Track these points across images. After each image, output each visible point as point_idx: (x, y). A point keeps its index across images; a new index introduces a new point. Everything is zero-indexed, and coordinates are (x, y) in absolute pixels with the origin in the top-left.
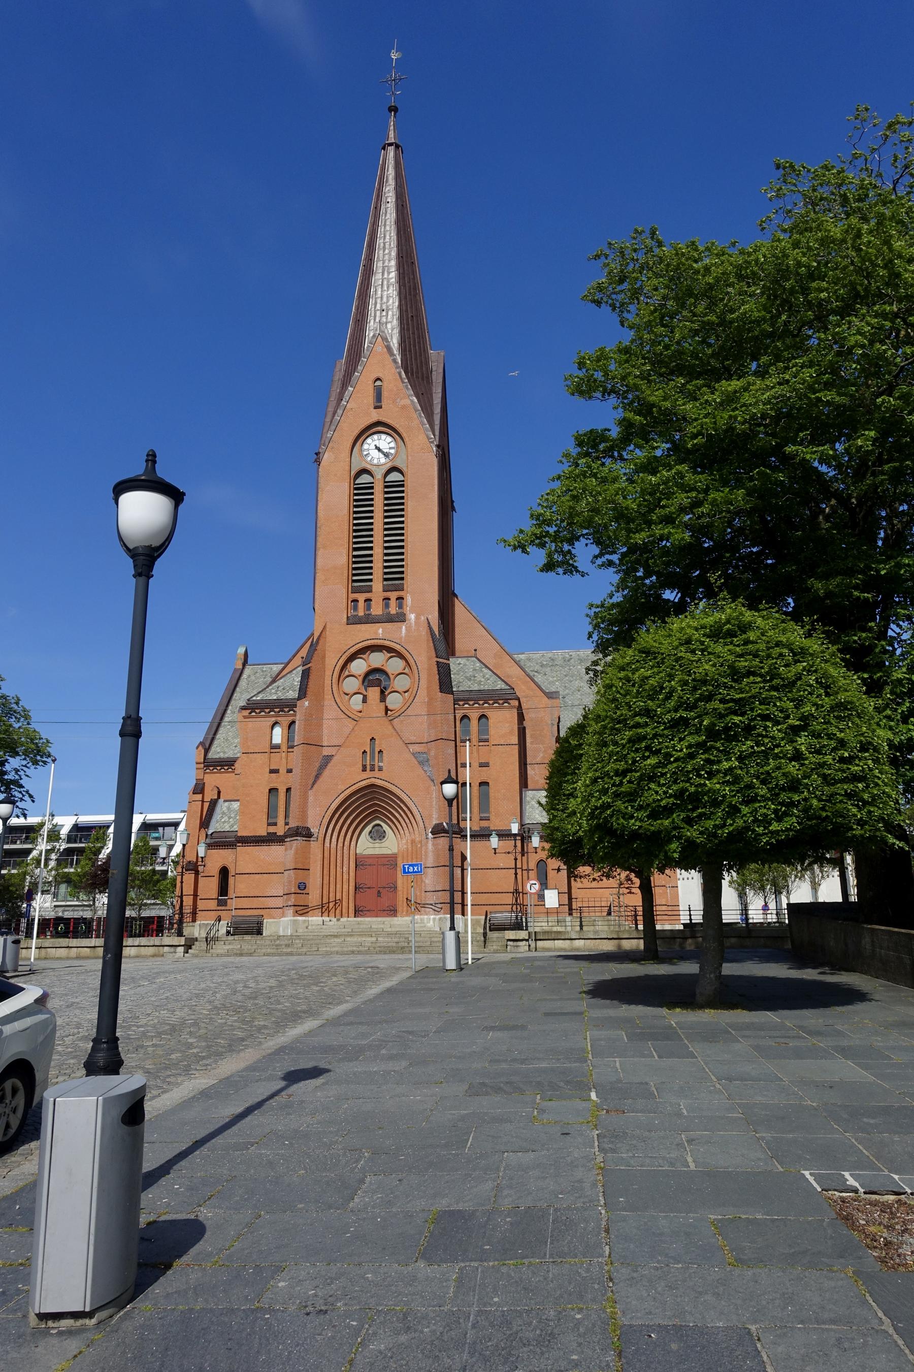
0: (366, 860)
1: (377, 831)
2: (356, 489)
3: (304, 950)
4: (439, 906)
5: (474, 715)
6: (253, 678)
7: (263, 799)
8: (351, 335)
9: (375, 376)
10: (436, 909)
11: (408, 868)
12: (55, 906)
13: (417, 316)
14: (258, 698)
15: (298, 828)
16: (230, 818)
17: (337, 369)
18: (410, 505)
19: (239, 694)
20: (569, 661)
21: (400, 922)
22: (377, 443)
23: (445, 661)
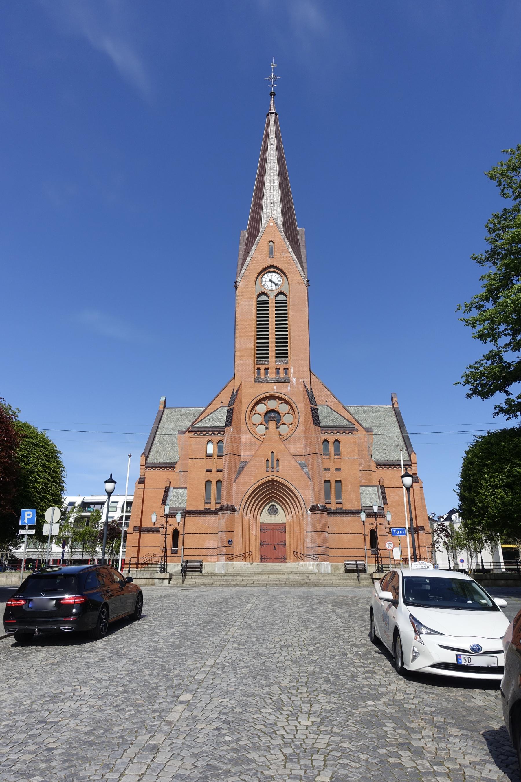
0: (266, 526)
1: (273, 509)
2: (258, 304)
3: (245, 583)
4: (316, 556)
5: (331, 439)
6: (170, 415)
7: (202, 487)
8: (251, 216)
9: (270, 239)
10: (314, 558)
11: (396, 532)
12: (28, 552)
13: (290, 208)
14: (198, 426)
15: (227, 505)
16: (178, 498)
17: (242, 236)
18: (292, 314)
19: (162, 425)
20: (358, 411)
21: (291, 566)
22: (270, 277)
23: (315, 407)
